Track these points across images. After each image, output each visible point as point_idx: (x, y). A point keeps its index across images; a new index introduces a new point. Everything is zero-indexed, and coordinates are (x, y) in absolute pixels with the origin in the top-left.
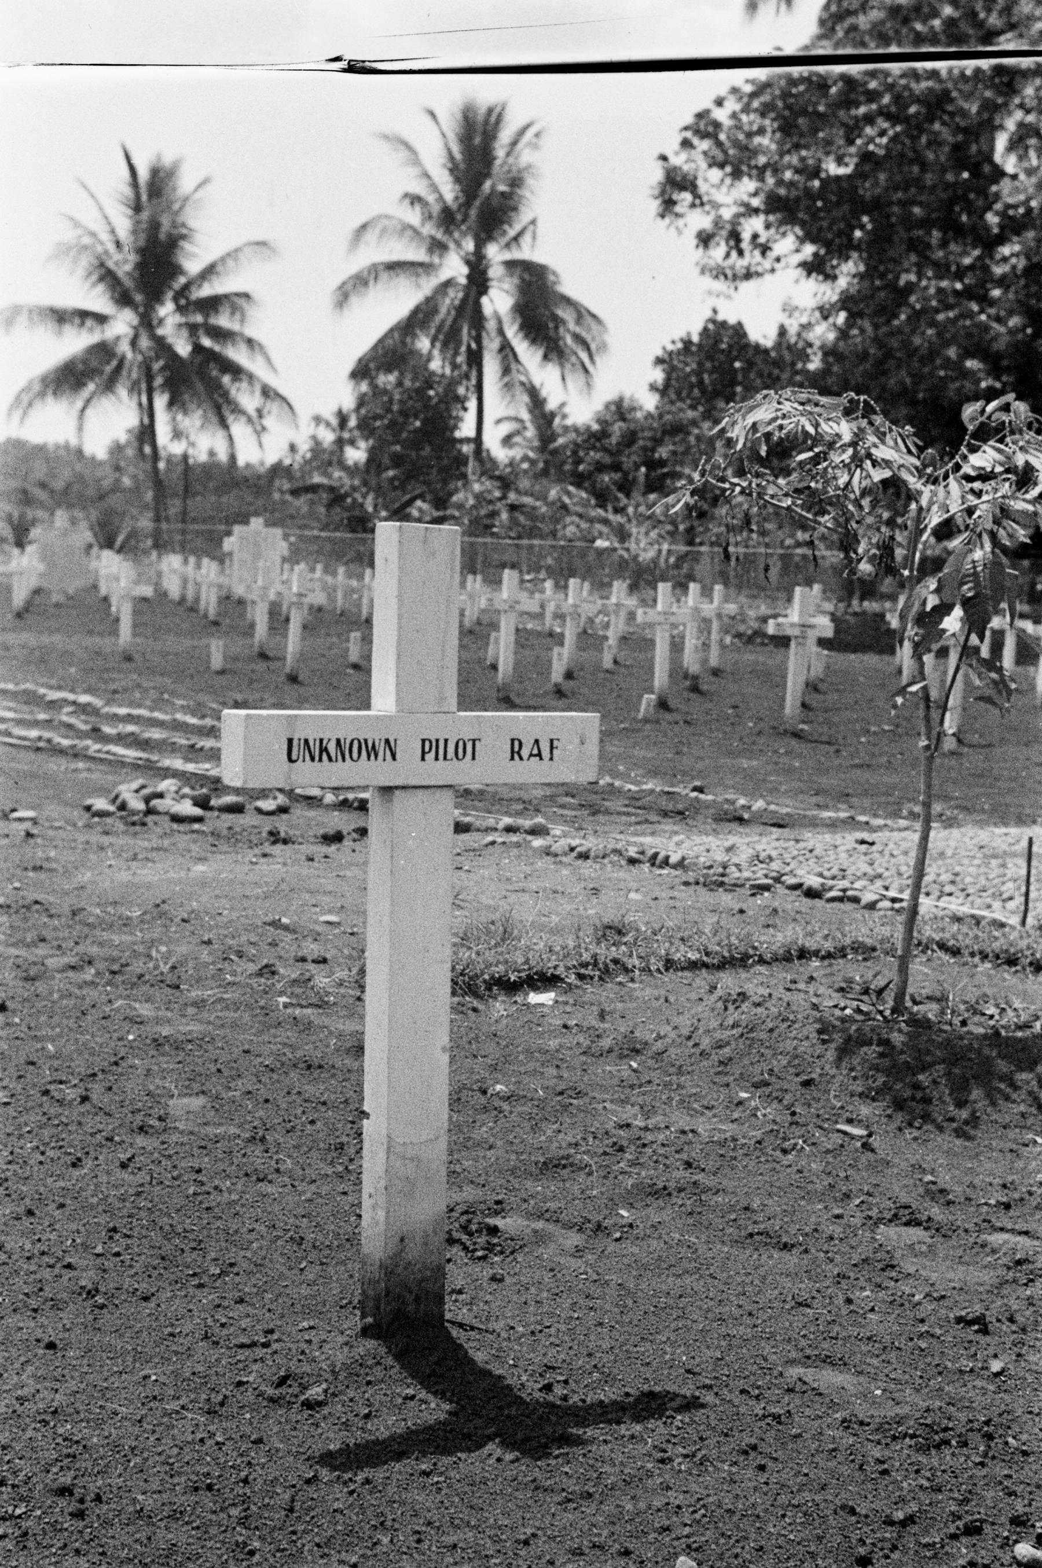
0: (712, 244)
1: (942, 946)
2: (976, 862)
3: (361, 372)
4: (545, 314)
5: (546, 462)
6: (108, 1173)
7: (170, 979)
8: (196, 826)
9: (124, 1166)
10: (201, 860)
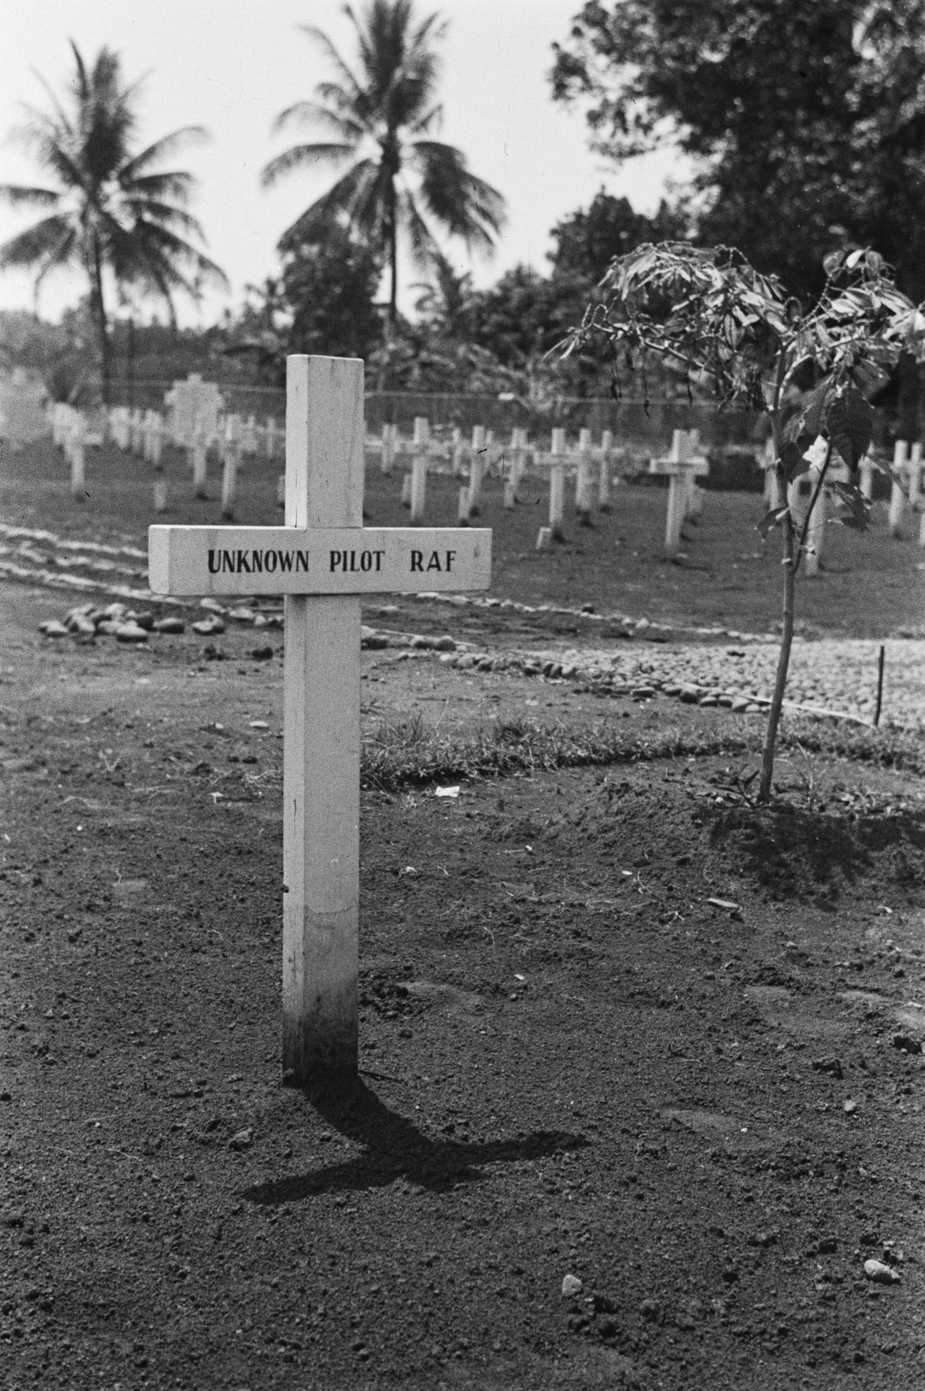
0: (600, 123)
1: (804, 743)
2: (834, 670)
3: (288, 243)
4: (452, 189)
5: (454, 325)
6: (59, 948)
7: (116, 777)
8: (140, 645)
9: (72, 940)
10: (146, 674)
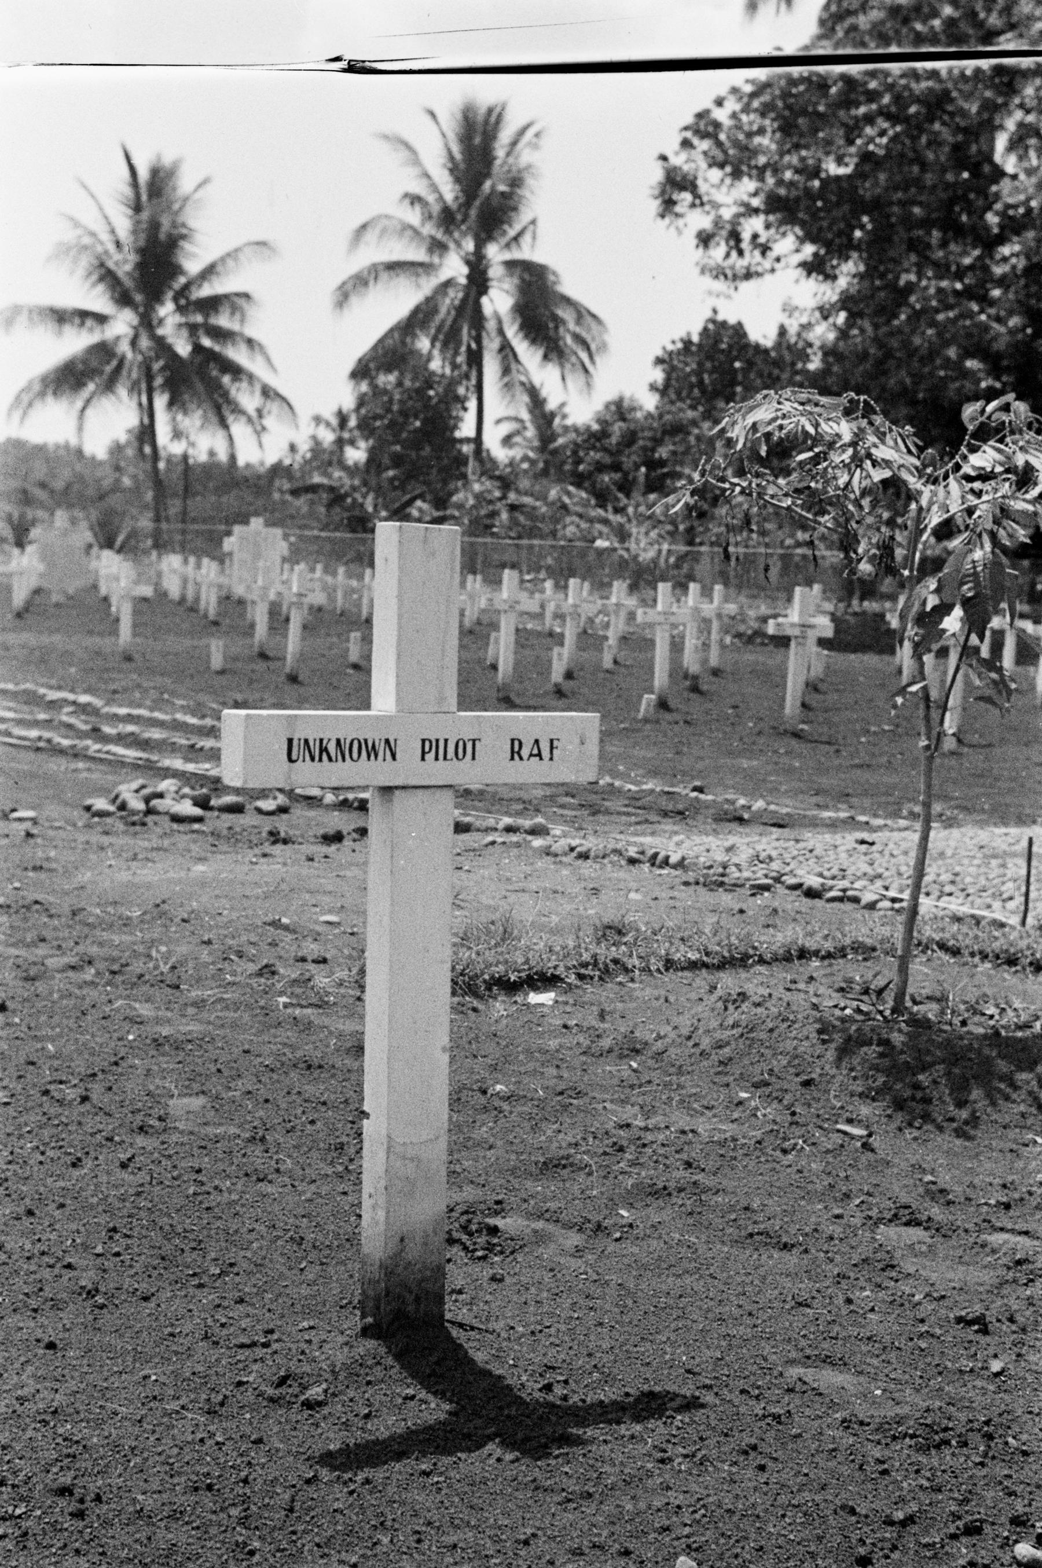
0: (712, 244)
1: (942, 946)
2: (976, 862)
3: (361, 372)
4: (545, 314)
5: (546, 462)
6: (108, 1173)
7: (170, 979)
8: (196, 826)
9: (124, 1166)
10: (201, 860)
